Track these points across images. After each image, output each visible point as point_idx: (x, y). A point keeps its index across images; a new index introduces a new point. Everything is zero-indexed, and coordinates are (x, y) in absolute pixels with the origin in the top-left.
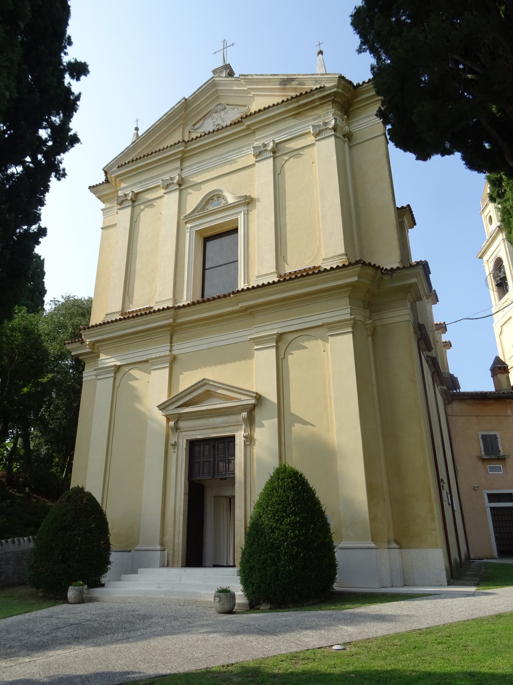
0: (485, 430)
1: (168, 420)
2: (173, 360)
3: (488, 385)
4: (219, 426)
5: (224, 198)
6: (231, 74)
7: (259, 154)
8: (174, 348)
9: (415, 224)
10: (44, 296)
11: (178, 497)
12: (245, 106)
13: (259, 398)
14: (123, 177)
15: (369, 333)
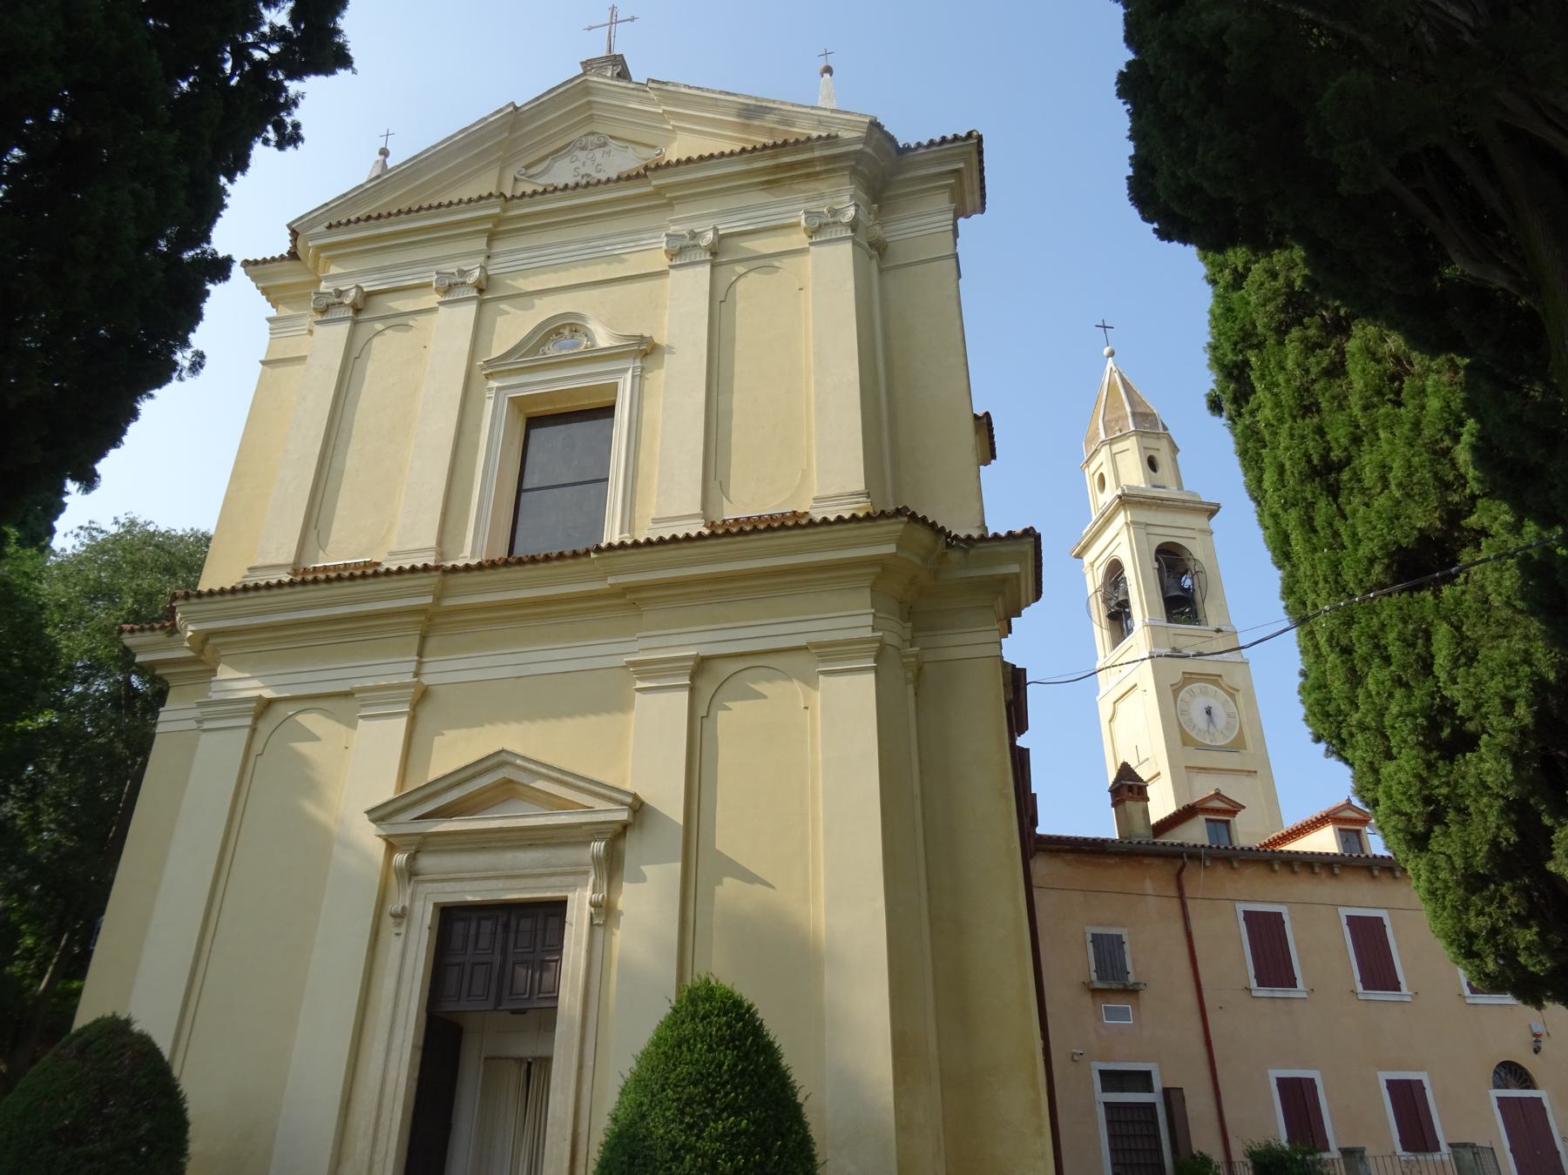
0: (1100, 924)
1: (391, 848)
2: (422, 696)
3: (1103, 825)
4: (528, 871)
5: (588, 335)
6: (624, 75)
7: (680, 252)
8: (426, 669)
9: (994, 457)
10: (56, 518)
11: (394, 1055)
12: (654, 147)
13: (638, 808)
14: (335, 252)
15: (910, 675)
